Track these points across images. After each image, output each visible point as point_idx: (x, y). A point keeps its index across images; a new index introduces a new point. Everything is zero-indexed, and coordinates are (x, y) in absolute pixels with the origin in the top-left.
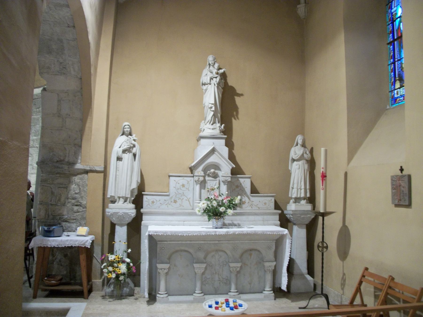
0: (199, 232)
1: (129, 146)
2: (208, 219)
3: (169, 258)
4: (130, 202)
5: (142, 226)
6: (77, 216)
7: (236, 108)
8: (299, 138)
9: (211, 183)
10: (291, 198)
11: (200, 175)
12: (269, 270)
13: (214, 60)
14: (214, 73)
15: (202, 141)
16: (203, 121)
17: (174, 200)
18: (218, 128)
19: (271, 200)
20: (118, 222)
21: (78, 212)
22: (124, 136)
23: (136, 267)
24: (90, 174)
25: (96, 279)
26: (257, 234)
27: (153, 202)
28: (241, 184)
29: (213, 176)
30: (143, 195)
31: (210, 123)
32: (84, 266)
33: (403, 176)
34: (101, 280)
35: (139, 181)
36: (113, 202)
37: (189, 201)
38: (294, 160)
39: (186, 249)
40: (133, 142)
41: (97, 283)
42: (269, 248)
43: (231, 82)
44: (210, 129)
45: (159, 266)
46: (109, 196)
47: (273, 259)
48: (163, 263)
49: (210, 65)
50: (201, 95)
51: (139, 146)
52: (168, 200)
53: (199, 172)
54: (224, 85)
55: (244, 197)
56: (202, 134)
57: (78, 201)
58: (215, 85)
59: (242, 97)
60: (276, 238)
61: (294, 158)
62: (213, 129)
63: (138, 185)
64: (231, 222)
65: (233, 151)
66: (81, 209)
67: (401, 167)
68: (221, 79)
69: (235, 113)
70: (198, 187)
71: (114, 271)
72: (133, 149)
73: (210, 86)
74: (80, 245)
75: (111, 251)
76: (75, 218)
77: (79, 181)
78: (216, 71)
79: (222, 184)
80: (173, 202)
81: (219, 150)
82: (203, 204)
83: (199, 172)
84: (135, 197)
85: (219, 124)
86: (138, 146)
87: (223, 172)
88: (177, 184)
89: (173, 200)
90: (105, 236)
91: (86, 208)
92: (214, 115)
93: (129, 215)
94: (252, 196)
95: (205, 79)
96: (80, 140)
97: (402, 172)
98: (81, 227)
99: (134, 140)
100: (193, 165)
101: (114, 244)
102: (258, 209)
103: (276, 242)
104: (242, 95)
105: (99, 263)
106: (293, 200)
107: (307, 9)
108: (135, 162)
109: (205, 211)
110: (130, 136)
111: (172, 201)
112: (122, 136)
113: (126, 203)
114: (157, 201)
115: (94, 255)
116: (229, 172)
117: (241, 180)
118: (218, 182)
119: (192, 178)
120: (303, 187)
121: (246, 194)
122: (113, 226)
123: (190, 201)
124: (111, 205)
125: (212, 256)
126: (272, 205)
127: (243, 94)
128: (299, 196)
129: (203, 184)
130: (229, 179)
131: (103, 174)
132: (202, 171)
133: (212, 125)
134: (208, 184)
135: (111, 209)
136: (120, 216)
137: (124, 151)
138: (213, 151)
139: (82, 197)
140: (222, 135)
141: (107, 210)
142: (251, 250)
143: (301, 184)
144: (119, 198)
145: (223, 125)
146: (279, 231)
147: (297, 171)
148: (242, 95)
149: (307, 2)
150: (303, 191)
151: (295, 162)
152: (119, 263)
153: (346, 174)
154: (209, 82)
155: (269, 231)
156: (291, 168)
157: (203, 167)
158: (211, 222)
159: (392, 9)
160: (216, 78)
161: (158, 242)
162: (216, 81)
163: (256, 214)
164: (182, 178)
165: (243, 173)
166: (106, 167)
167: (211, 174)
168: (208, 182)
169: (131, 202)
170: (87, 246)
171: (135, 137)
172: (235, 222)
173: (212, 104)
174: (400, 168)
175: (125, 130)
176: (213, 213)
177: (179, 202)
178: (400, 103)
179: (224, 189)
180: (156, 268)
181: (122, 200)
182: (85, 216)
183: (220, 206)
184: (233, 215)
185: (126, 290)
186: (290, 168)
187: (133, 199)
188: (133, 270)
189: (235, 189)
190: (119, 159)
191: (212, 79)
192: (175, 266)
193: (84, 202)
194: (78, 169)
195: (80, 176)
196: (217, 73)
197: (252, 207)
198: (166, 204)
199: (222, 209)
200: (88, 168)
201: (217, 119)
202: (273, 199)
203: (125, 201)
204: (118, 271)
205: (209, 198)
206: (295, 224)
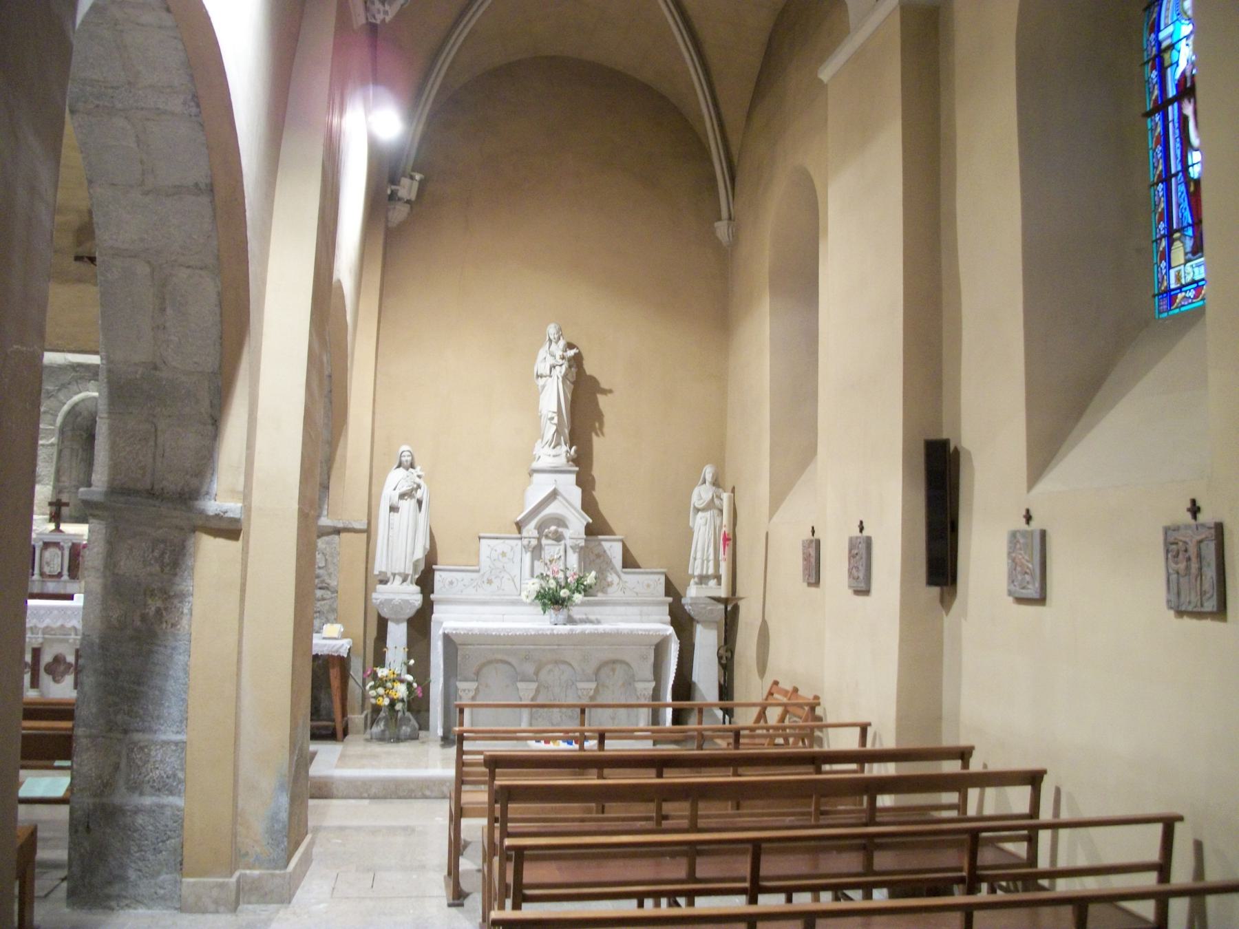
0: (525, 629)
1: (410, 486)
2: (543, 609)
3: (477, 673)
4: (411, 583)
5: (432, 624)
6: (321, 605)
7: (599, 416)
8: (707, 471)
9: (552, 550)
10: (693, 576)
11: (531, 536)
12: (644, 695)
13: (558, 333)
14: (558, 357)
15: (536, 476)
16: (540, 441)
17: (488, 580)
18: (564, 454)
19: (659, 580)
20: (393, 616)
21: (323, 599)
22: (401, 469)
23: (422, 689)
24: (343, 535)
25: (353, 714)
26: (621, 633)
27: (451, 583)
28: (605, 551)
29: (555, 537)
30: (433, 571)
31: (550, 446)
32: (338, 687)
33: (1032, 533)
34: (363, 716)
35: (428, 546)
36: (384, 582)
37: (513, 580)
38: (698, 510)
39: (506, 658)
40: (418, 480)
41: (357, 720)
42: (644, 658)
43: (590, 368)
44: (550, 455)
45: (461, 685)
46: (376, 572)
47: (651, 677)
48: (466, 680)
49: (550, 340)
50: (536, 394)
51: (427, 485)
52: (476, 579)
53: (530, 530)
54: (575, 377)
55: (611, 574)
56: (536, 465)
57: (323, 581)
58: (558, 378)
59: (609, 395)
60: (657, 641)
61: (697, 506)
62: (554, 456)
63: (426, 553)
64: (584, 617)
65: (594, 493)
66: (327, 594)
67: (1194, 502)
68: (570, 367)
69: (597, 425)
70: (527, 557)
71: (388, 695)
72: (416, 492)
73: (550, 380)
74: (330, 653)
75: (380, 660)
76: (318, 610)
77: (324, 546)
78: (561, 353)
79: (570, 551)
80: (486, 581)
81: (564, 494)
82: (533, 586)
83: (530, 530)
84: (420, 574)
85: (565, 446)
86: (426, 487)
87: (571, 531)
88: (494, 552)
89: (485, 579)
90: (368, 642)
91: (337, 592)
92: (557, 431)
93: (410, 604)
94: (625, 573)
95: (542, 366)
96: (326, 476)
97: (1195, 517)
98: (329, 625)
99: (419, 477)
100: (518, 519)
101: (385, 652)
102: (635, 595)
103: (655, 649)
104: (610, 391)
105: (359, 686)
106: (696, 579)
107: (732, 231)
108: (420, 515)
109: (537, 597)
110: (411, 470)
111: (483, 582)
112: (398, 469)
113: (405, 583)
114: (457, 580)
115: (351, 673)
116: (583, 530)
117: (606, 545)
118: (562, 548)
119: (519, 542)
120: (712, 557)
121: (613, 568)
122: (382, 624)
123: (515, 580)
124: (380, 587)
125: (550, 671)
126: (661, 588)
127: (613, 389)
128: (704, 572)
129: (537, 551)
130: (582, 543)
131: (364, 536)
132: (535, 528)
133: (554, 448)
134: (547, 552)
135: (381, 594)
136: (396, 605)
137: (402, 496)
138: (554, 495)
139: (330, 575)
140: (571, 466)
141: (374, 595)
142: (614, 662)
143: (709, 552)
144: (394, 575)
145: (574, 448)
146: (659, 630)
147: (703, 529)
148: (610, 391)
149: (732, 218)
150: (711, 564)
151: (700, 513)
152: (394, 681)
153: (767, 534)
154: (548, 373)
155: (641, 630)
156: (694, 526)
157: (537, 523)
158: (547, 616)
159: (1159, 31)
160: (561, 365)
161: (459, 647)
162: (560, 371)
163: (628, 604)
164: (502, 541)
165: (611, 532)
166: (369, 523)
167: (550, 535)
168: (546, 548)
169: (414, 582)
170: (341, 655)
171: (420, 470)
172: (592, 617)
173: (554, 412)
174: (1189, 505)
175: (403, 459)
176: (550, 600)
177: (496, 582)
178: (1183, 309)
179: (573, 560)
180: (457, 689)
181: (398, 579)
182: (335, 606)
183: (562, 588)
184: (583, 604)
185: (406, 730)
186: (691, 524)
187: (417, 576)
188: (419, 693)
189: (594, 561)
190: (393, 509)
191: (554, 367)
192: (487, 686)
193: (333, 583)
194: (323, 526)
195: (325, 538)
196: (563, 358)
197: (624, 592)
198: (474, 587)
199: (564, 593)
200: (340, 525)
201: (562, 438)
202: (663, 579)
203: (404, 580)
204: (393, 694)
205: (542, 574)
206: (698, 622)
